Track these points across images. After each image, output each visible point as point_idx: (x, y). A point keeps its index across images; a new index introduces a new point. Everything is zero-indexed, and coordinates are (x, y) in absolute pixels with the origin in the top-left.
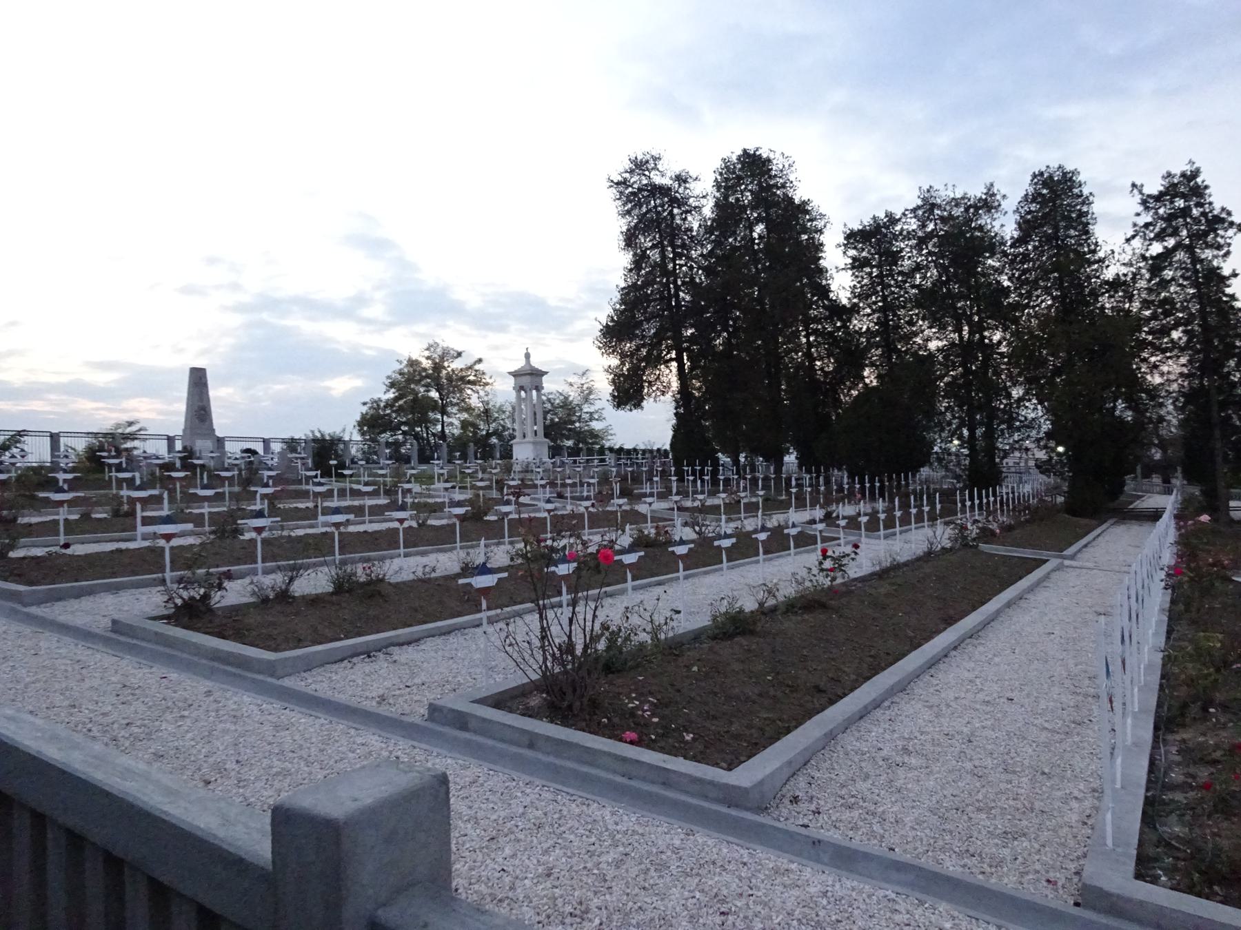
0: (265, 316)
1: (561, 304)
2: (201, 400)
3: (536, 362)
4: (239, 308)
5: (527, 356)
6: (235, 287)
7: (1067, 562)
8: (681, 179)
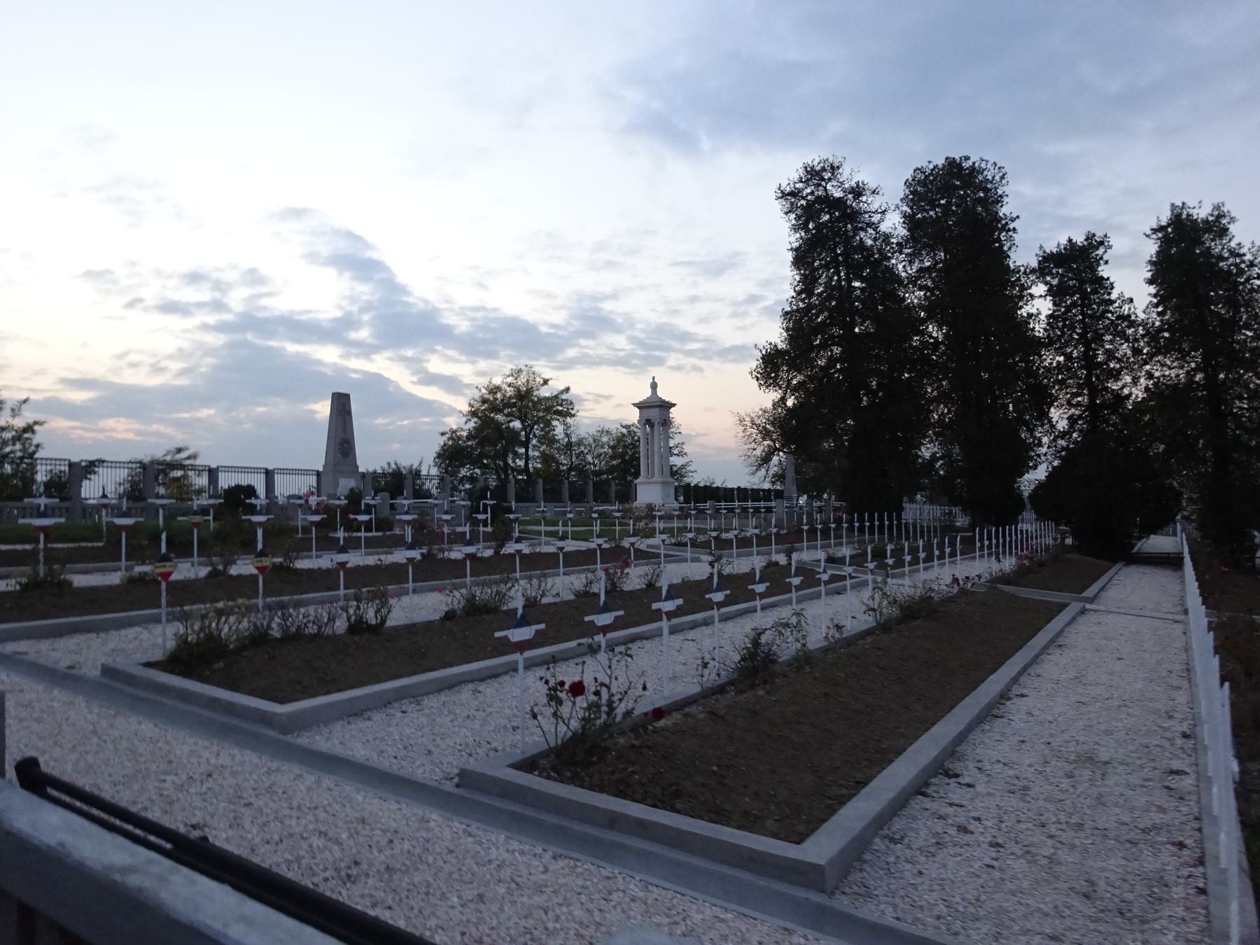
0: (249, 336)
1: (552, 331)
2: (345, 431)
3: (663, 394)
4: (221, 328)
5: (654, 386)
6: (218, 306)
8: (857, 192)
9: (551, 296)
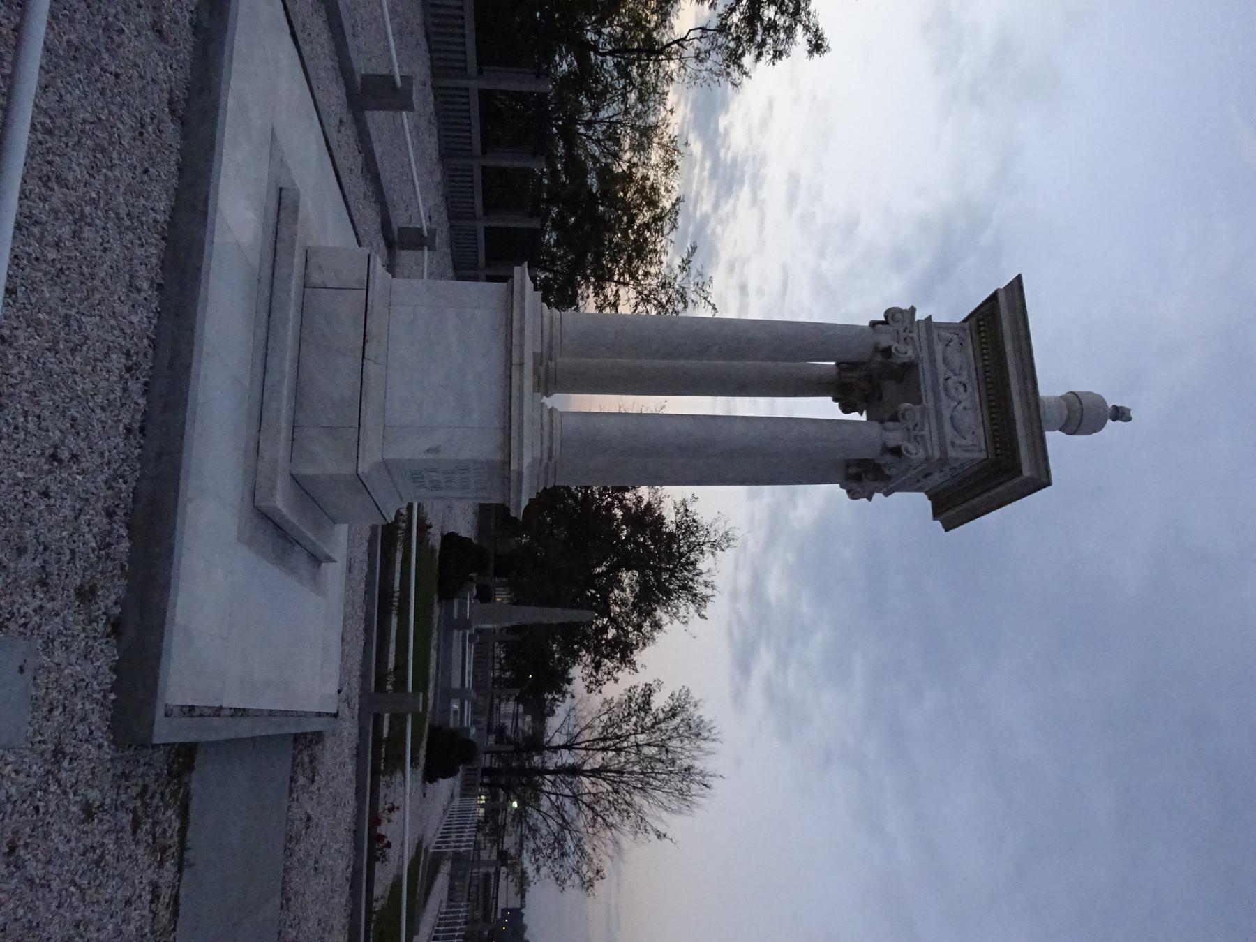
9: (764, 123)
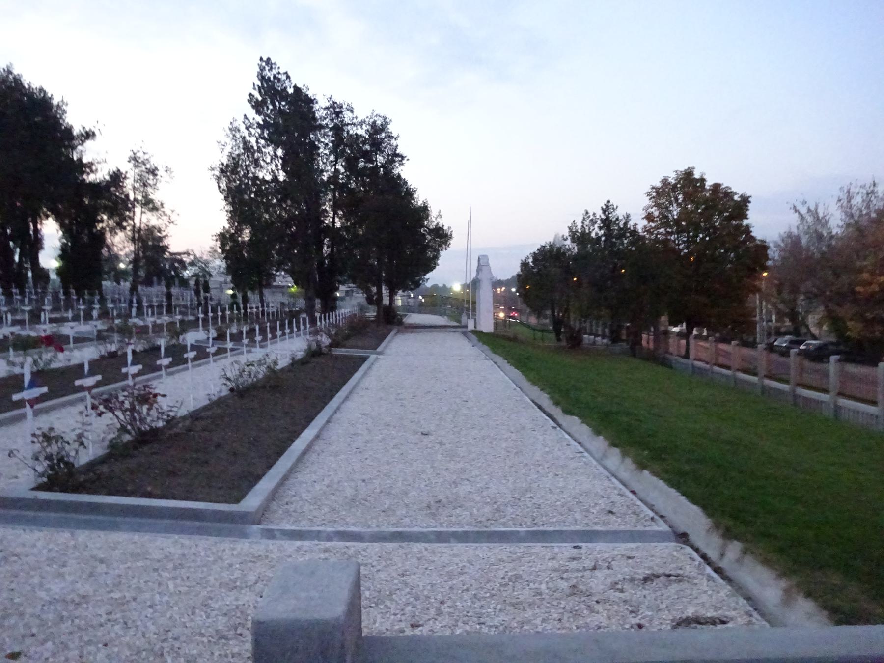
7: (381, 357)
